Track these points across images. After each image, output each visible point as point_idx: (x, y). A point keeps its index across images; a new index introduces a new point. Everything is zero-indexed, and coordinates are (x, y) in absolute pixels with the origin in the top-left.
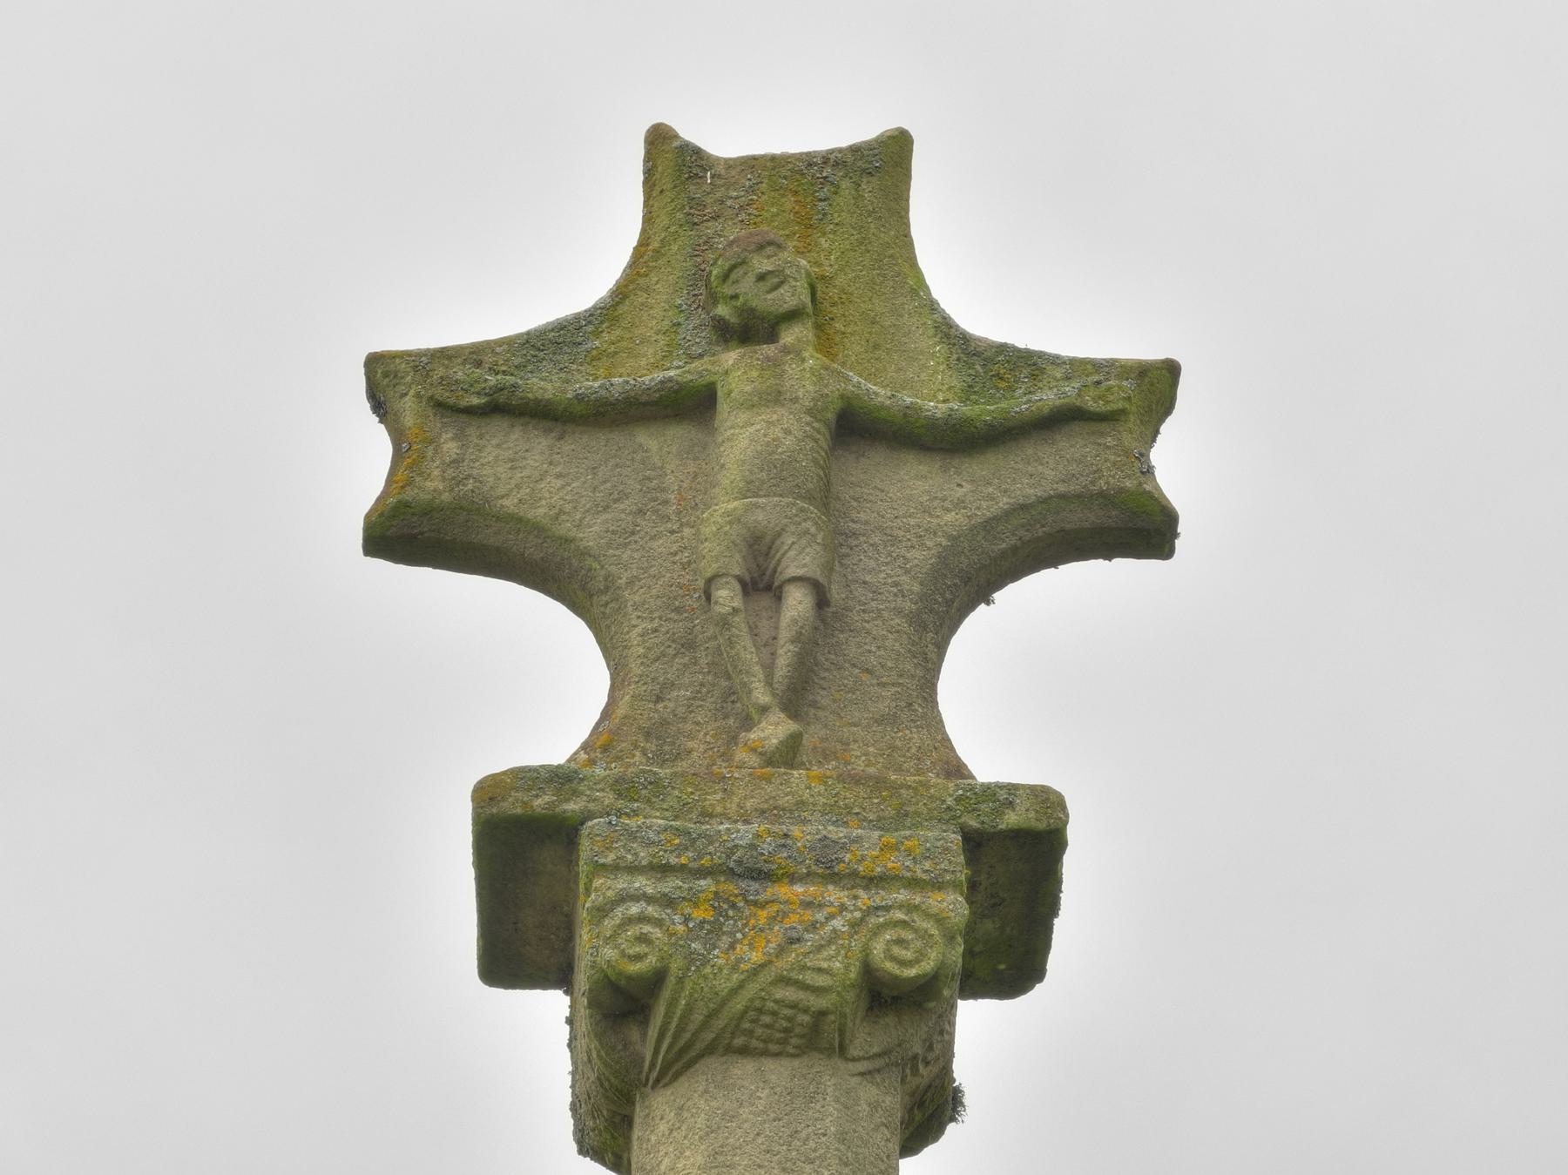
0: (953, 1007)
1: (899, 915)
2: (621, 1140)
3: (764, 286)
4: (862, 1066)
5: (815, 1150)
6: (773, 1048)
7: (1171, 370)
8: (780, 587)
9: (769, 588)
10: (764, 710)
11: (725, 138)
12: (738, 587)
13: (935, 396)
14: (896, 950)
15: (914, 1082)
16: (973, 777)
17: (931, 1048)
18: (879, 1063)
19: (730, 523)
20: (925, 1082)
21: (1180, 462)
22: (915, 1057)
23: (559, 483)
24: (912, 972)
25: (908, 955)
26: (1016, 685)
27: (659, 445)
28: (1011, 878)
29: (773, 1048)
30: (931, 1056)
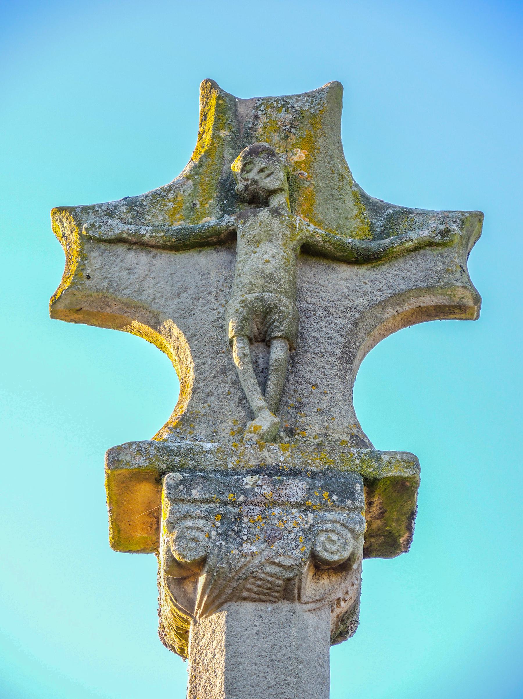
0: (324, 661)
1: (329, 525)
2: (183, 641)
3: (263, 175)
4: (312, 606)
5: (285, 655)
6: (263, 597)
7: (479, 216)
8: (269, 341)
9: (263, 340)
10: (260, 409)
11: (245, 88)
12: (247, 342)
13: (353, 233)
14: (328, 545)
15: (338, 611)
16: (371, 446)
17: (347, 593)
18: (319, 605)
19: (242, 307)
20: (345, 610)
21: (483, 266)
22: (339, 599)
23: (154, 282)
24: (336, 558)
25: (334, 548)
26: (397, 392)
27: (207, 260)
28: (389, 508)
29: (263, 597)
30: (347, 598)
